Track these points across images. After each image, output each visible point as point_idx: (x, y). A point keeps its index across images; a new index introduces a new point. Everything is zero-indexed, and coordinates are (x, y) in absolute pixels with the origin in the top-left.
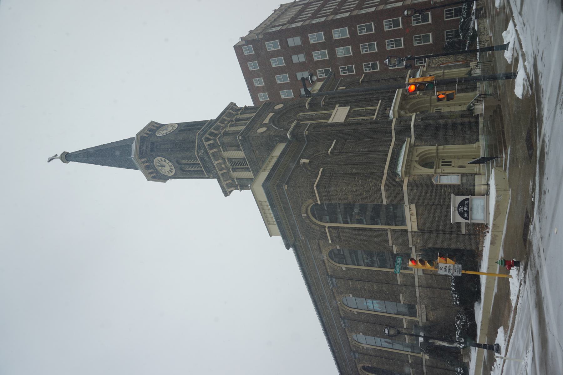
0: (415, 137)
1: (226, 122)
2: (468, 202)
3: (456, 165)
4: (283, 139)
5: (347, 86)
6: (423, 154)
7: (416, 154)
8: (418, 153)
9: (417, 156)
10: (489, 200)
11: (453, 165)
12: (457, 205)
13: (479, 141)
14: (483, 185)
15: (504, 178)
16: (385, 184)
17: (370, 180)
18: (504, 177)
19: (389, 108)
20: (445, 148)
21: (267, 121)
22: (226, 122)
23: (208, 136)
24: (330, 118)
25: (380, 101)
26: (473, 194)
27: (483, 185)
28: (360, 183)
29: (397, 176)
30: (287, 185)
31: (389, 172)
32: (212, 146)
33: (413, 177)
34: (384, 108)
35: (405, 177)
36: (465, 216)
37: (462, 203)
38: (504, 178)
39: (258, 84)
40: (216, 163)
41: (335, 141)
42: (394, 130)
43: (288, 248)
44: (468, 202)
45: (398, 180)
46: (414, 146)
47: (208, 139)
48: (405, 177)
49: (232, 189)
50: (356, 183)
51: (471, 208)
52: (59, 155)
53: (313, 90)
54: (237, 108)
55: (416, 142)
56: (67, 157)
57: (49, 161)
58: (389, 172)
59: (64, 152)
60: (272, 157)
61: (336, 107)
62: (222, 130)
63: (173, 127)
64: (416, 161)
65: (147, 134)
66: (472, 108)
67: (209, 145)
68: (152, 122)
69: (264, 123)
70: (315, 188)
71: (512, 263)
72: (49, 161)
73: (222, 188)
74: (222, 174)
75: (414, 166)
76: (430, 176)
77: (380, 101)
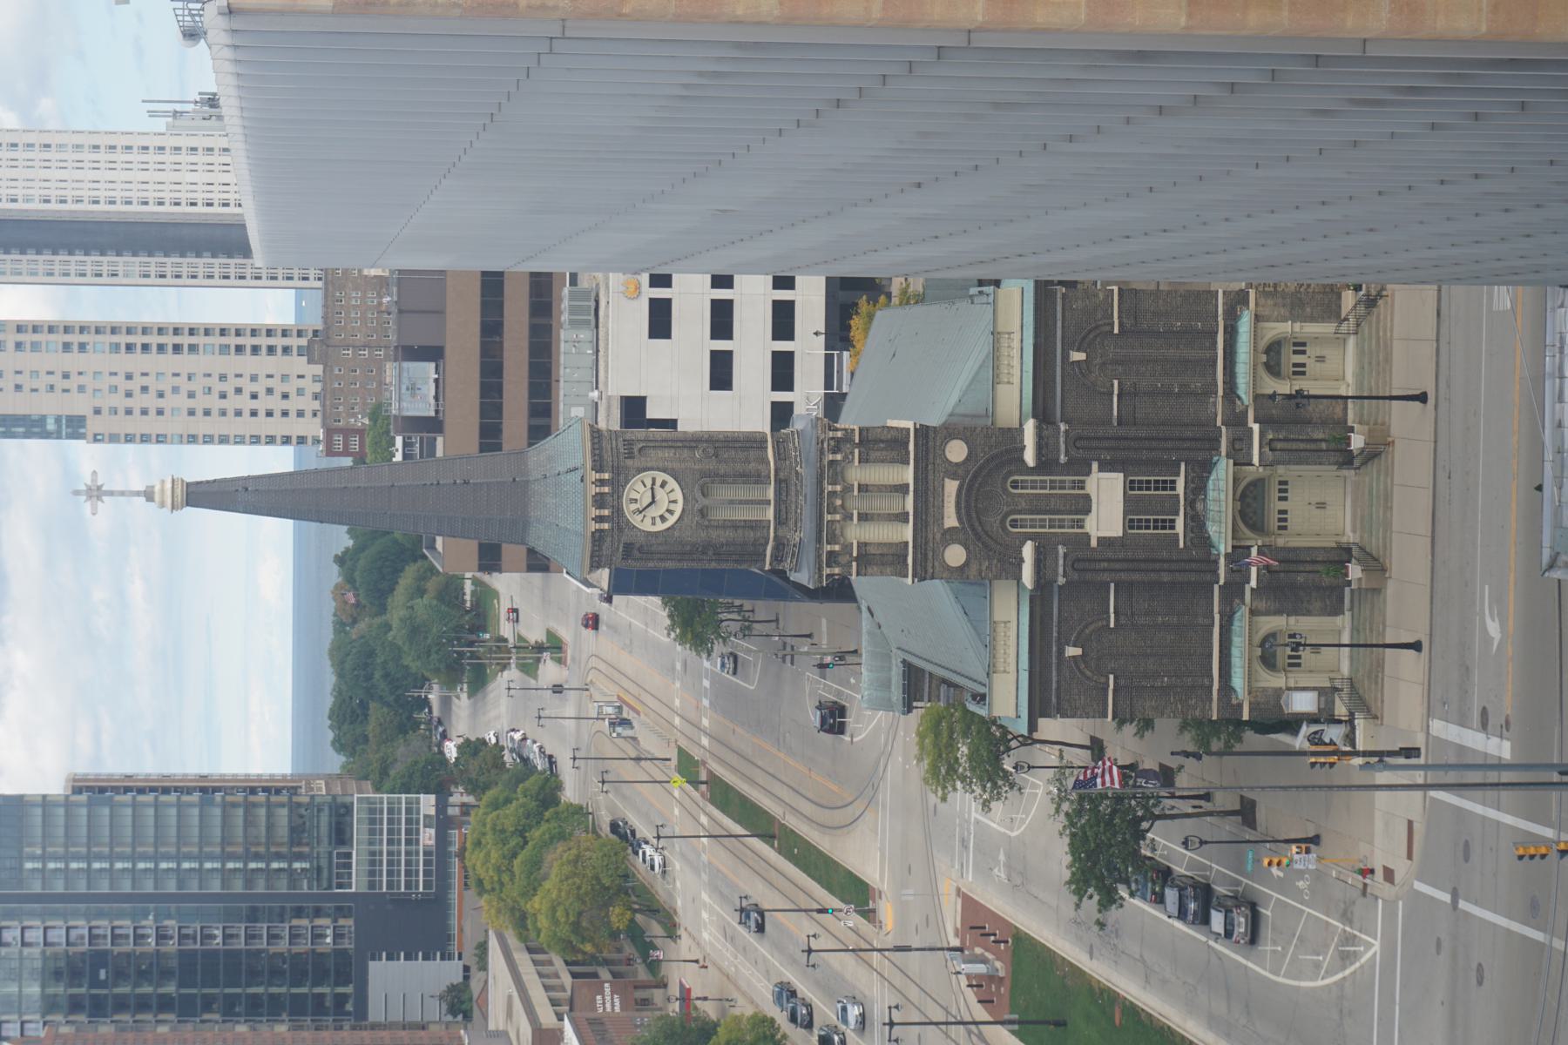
21: (951, 521)
45: (1234, 702)
76: (1278, 693)
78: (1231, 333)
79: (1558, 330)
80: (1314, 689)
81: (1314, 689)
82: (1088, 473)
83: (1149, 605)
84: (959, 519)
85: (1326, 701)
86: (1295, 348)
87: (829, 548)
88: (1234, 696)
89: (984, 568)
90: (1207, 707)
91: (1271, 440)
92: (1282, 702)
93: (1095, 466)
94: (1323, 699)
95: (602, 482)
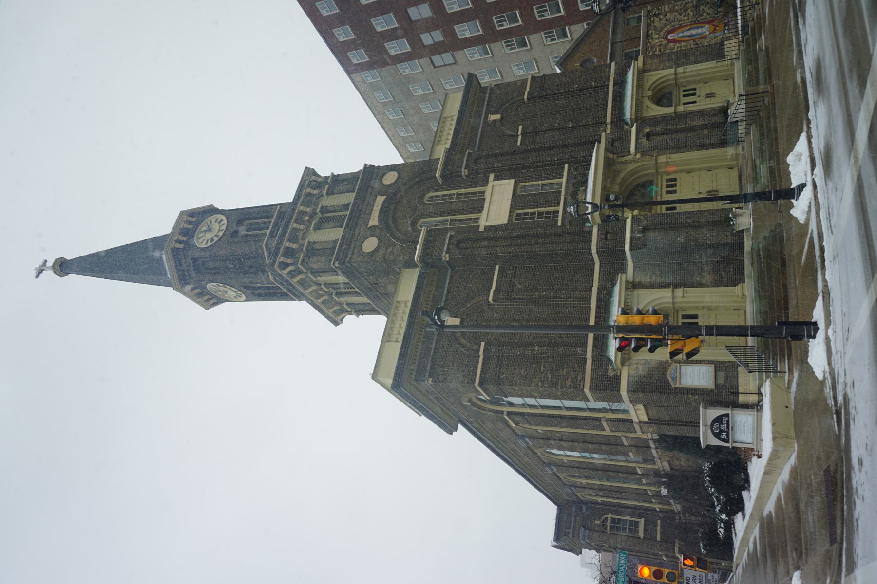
0: (634, 263)
1: (307, 218)
2: (727, 418)
3: (703, 94)
4: (410, 264)
5: (503, 111)
6: (659, 82)
7: (647, 85)
8: (650, 82)
9: (649, 89)
10: (761, 420)
11: (698, 94)
12: (709, 422)
13: (744, 282)
14: (752, 393)
15: (787, 407)
16: (591, 380)
17: (564, 372)
18: (787, 405)
19: (584, 188)
20: (687, 295)
21: (374, 221)
22: (307, 218)
23: (282, 259)
24: (483, 210)
25: (566, 166)
26: (736, 405)
27: (752, 393)
28: (549, 379)
29: (609, 365)
30: (431, 379)
31: (594, 353)
32: (292, 274)
33: (635, 366)
34: (574, 184)
35: (622, 366)
36: (723, 437)
37: (718, 420)
38: (787, 407)
39: (344, 37)
40: (308, 291)
41: (497, 267)
42: (596, 255)
43: (452, 434)
44: (727, 418)
45: (611, 373)
46: (644, 71)
47: (284, 265)
48: (622, 366)
49: (344, 315)
50: (542, 378)
51: (732, 427)
52: (50, 264)
53: (445, 118)
54: (319, 180)
55: (636, 273)
56: (63, 267)
57: (37, 276)
58: (594, 353)
59: (56, 260)
60: (397, 304)
61: (490, 180)
62: (302, 239)
63: (219, 223)
64: (648, 97)
65: (180, 242)
66: (732, 223)
67: (289, 273)
68: (182, 213)
69: (370, 225)
70: (478, 388)
71: (812, 328)
72: (37, 276)
73: (328, 317)
74: (324, 302)
75: (647, 106)
77: (566, 166)
78: (620, 83)
79: (836, 546)
80: (709, 362)
81: (709, 362)
82: (486, 184)
83: (530, 284)
84: (379, 221)
85: (726, 378)
86: (685, 93)
87: (288, 244)
88: (610, 368)
89: (388, 252)
90: (579, 377)
91: (648, 133)
92: (668, 375)
93: (492, 176)
94: (721, 374)
95: (190, 223)
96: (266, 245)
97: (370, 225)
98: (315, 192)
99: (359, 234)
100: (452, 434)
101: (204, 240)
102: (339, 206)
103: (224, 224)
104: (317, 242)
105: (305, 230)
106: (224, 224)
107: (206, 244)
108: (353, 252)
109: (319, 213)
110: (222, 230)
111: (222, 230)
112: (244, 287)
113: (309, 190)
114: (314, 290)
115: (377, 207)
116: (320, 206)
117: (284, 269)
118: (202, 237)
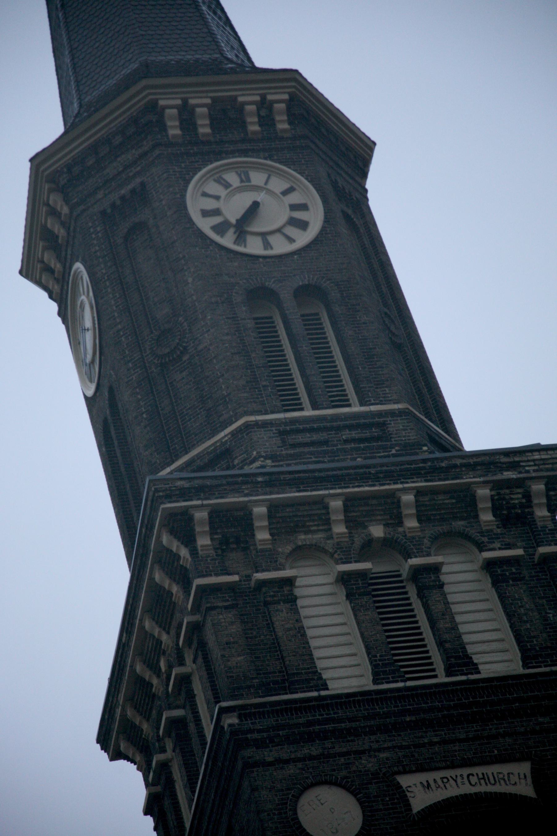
43: (146, 814)
49: (138, 758)
69: (405, 781)
96: (247, 426)
97: (405, 781)
98: (487, 517)
99: (360, 753)
100: (146, 814)
101: (217, 198)
102: (454, 627)
103: (291, 240)
104: (297, 612)
105: (329, 545)
106: (291, 240)
107: (206, 213)
108: (287, 762)
109: (407, 567)
110: (267, 245)
111: (267, 245)
112: (111, 390)
113: (483, 492)
114: (159, 642)
115: (484, 778)
116: (439, 559)
117: (173, 532)
118: (227, 185)
